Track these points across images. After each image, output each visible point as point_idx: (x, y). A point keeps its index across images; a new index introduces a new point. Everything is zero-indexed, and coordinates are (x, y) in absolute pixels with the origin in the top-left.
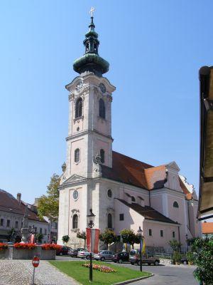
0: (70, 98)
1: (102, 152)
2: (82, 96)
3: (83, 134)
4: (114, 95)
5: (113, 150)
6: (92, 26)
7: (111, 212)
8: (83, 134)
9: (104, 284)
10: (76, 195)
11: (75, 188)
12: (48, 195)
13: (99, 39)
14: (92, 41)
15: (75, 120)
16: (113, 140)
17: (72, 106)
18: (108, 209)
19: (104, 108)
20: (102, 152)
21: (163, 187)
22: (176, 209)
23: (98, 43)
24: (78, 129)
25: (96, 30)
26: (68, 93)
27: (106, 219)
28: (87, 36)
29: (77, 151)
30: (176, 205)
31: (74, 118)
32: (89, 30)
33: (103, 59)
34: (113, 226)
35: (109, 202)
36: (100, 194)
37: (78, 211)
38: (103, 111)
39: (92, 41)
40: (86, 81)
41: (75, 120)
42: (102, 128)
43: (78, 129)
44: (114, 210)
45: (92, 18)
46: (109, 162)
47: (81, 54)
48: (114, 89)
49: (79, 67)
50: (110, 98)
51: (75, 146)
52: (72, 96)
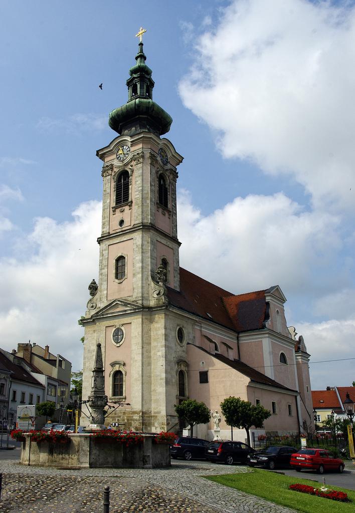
0: (104, 172)
1: (165, 263)
2: (128, 169)
3: (133, 230)
4: (179, 169)
5: (182, 265)
6: (142, 57)
7: (183, 368)
8: (133, 230)
9: (303, 512)
10: (118, 335)
11: (117, 322)
12: (155, 326)
13: (154, 77)
14: (141, 79)
15: (115, 209)
16: (180, 244)
17: (109, 185)
18: (180, 362)
19: (166, 190)
20: (165, 263)
21: (264, 327)
22: (283, 366)
23: (152, 84)
24: (122, 222)
25: (148, 63)
26: (100, 164)
27: (175, 379)
28: (133, 72)
29: (120, 259)
30: (283, 359)
31: (113, 204)
32: (137, 64)
33: (163, 111)
34: (187, 393)
35: (178, 351)
36: (166, 335)
37: (124, 365)
38: (164, 196)
39: (141, 79)
40: (133, 146)
41: (115, 209)
42: (163, 223)
43: (122, 222)
44: (187, 365)
45: (141, 44)
46: (174, 282)
47: (122, 99)
48: (180, 160)
49: (120, 122)
50: (176, 175)
51: (117, 251)
52: (106, 170)
